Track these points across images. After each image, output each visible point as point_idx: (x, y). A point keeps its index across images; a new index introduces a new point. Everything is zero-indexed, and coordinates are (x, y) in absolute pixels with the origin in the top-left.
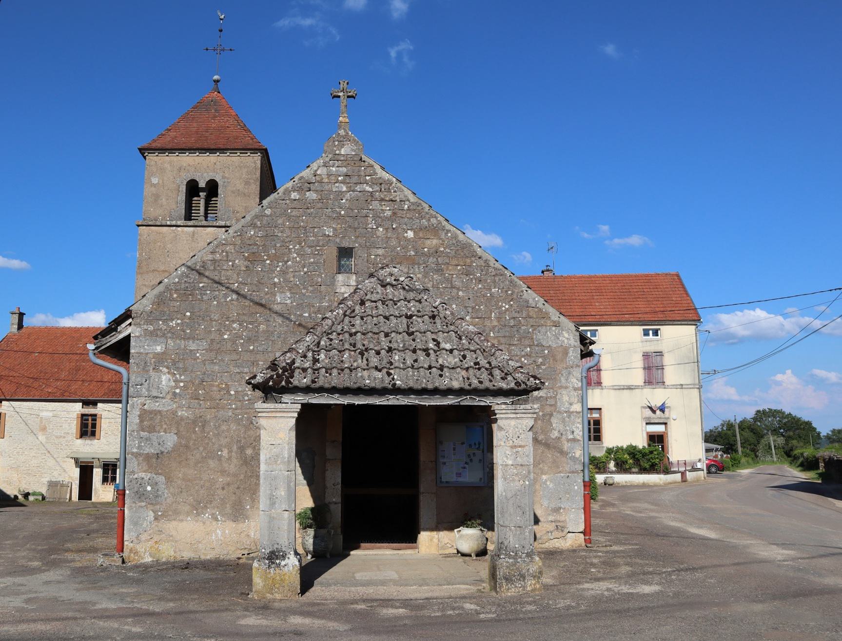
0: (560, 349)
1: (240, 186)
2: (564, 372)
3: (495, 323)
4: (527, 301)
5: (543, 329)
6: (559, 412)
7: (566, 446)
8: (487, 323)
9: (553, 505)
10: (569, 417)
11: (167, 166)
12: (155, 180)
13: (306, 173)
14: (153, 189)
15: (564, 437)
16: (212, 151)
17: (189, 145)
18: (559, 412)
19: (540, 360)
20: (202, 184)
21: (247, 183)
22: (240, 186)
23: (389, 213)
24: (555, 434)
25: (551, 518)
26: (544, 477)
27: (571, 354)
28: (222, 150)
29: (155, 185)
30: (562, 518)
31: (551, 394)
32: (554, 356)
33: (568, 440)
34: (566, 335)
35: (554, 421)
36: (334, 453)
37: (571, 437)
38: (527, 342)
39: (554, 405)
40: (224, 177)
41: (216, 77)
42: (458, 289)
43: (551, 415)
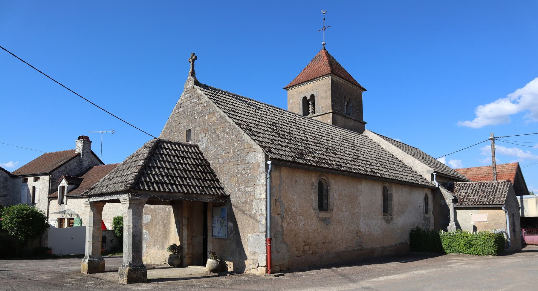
0: (257, 164)
1: (323, 94)
2: (258, 177)
3: (232, 155)
4: (244, 140)
5: (249, 154)
6: (256, 199)
7: (259, 218)
8: (230, 155)
9: (252, 251)
10: (260, 201)
11: (295, 93)
12: (291, 101)
13: (179, 101)
14: (291, 105)
15: (257, 213)
16: (310, 81)
17: (305, 80)
18: (256, 199)
19: (249, 171)
20: (308, 98)
21: (326, 92)
22: (323, 94)
23: (201, 109)
24: (254, 211)
25: (252, 257)
26: (249, 235)
27: (261, 166)
28: (314, 79)
29: (291, 104)
30: (256, 258)
31: (252, 190)
32: (254, 168)
33: (260, 215)
34: (259, 155)
35: (254, 204)
36: (185, 222)
37: (260, 213)
38: (243, 162)
39: (254, 195)
40: (316, 92)
41: (323, 43)
42: (220, 140)
43: (252, 201)
